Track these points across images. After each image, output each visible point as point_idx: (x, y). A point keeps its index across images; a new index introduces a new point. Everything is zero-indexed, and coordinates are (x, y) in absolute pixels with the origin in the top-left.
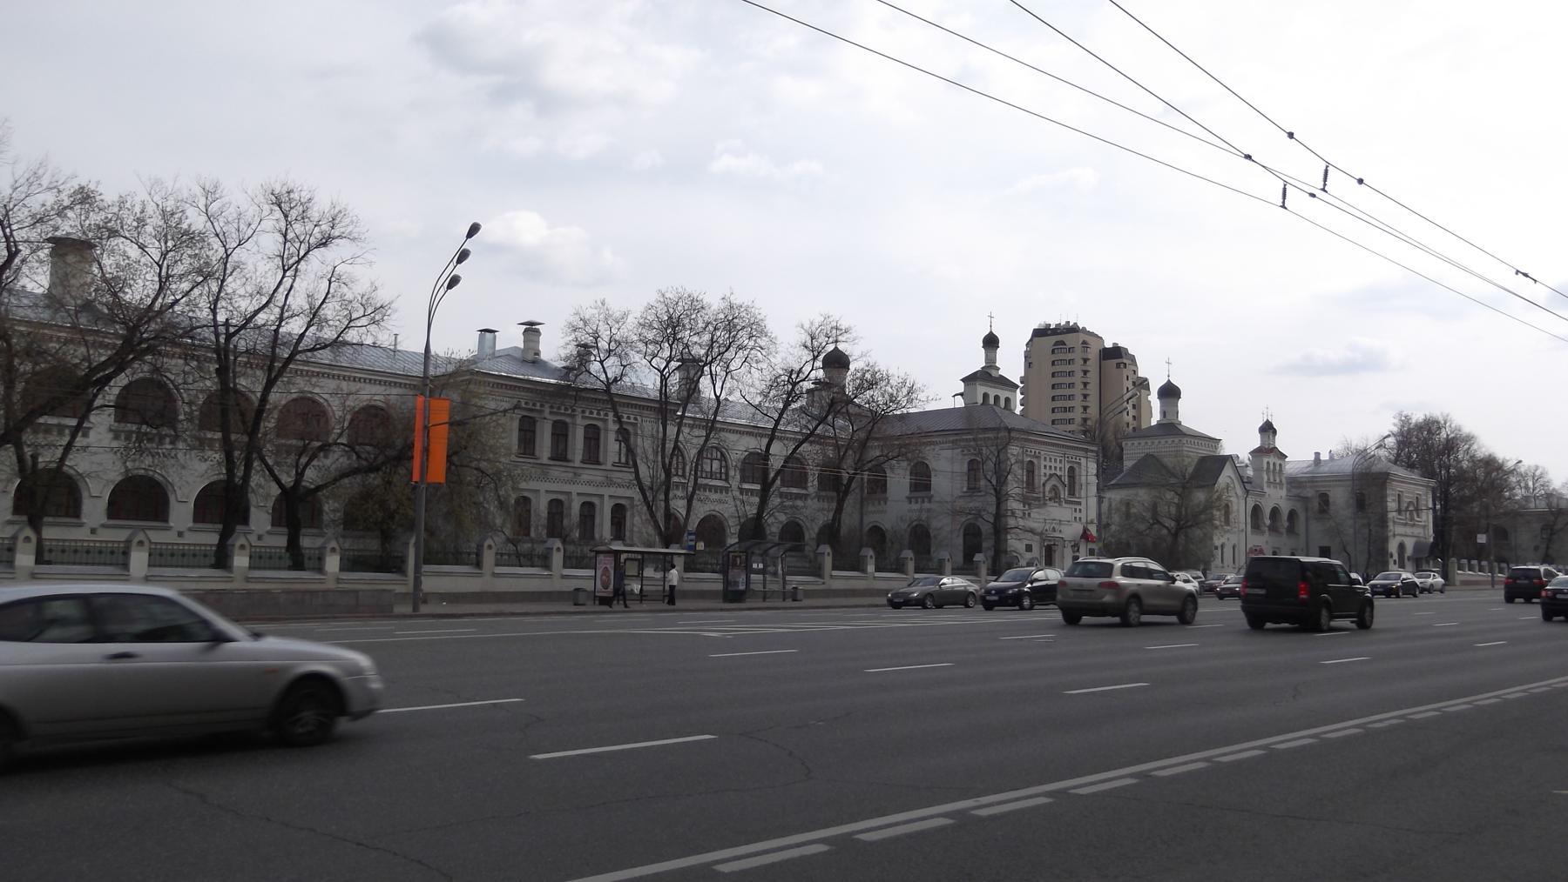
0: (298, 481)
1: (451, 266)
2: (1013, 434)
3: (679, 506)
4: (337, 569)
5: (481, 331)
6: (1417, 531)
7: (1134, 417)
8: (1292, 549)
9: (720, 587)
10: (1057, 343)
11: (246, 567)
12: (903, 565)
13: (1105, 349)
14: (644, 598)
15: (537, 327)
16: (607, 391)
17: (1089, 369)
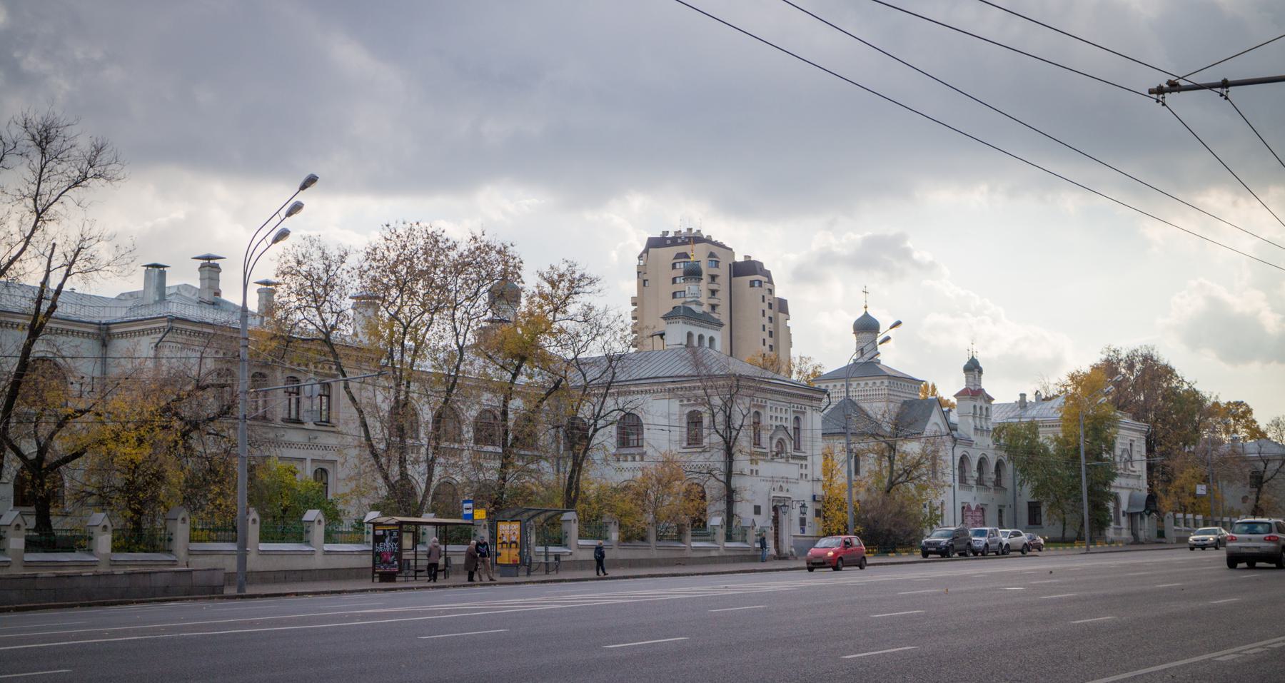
0: (42, 451)
1: (276, 220)
2: (742, 383)
3: (417, 473)
4: (109, 551)
5: (148, 266)
6: (1132, 482)
7: (771, 346)
8: (999, 506)
9: (367, 561)
10: (679, 256)
11: (21, 550)
12: (307, 532)
13: (735, 263)
14: (418, 574)
15: (216, 261)
16: (327, 341)
17: (1100, 354)
